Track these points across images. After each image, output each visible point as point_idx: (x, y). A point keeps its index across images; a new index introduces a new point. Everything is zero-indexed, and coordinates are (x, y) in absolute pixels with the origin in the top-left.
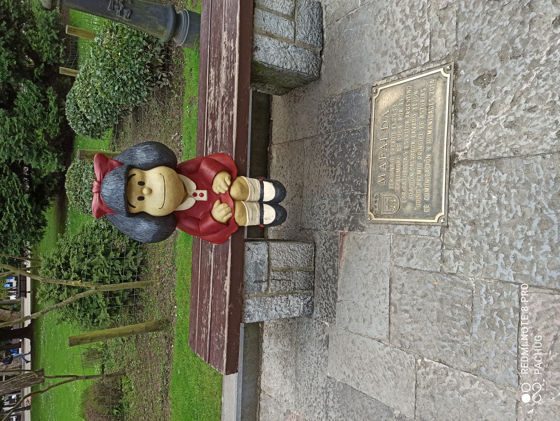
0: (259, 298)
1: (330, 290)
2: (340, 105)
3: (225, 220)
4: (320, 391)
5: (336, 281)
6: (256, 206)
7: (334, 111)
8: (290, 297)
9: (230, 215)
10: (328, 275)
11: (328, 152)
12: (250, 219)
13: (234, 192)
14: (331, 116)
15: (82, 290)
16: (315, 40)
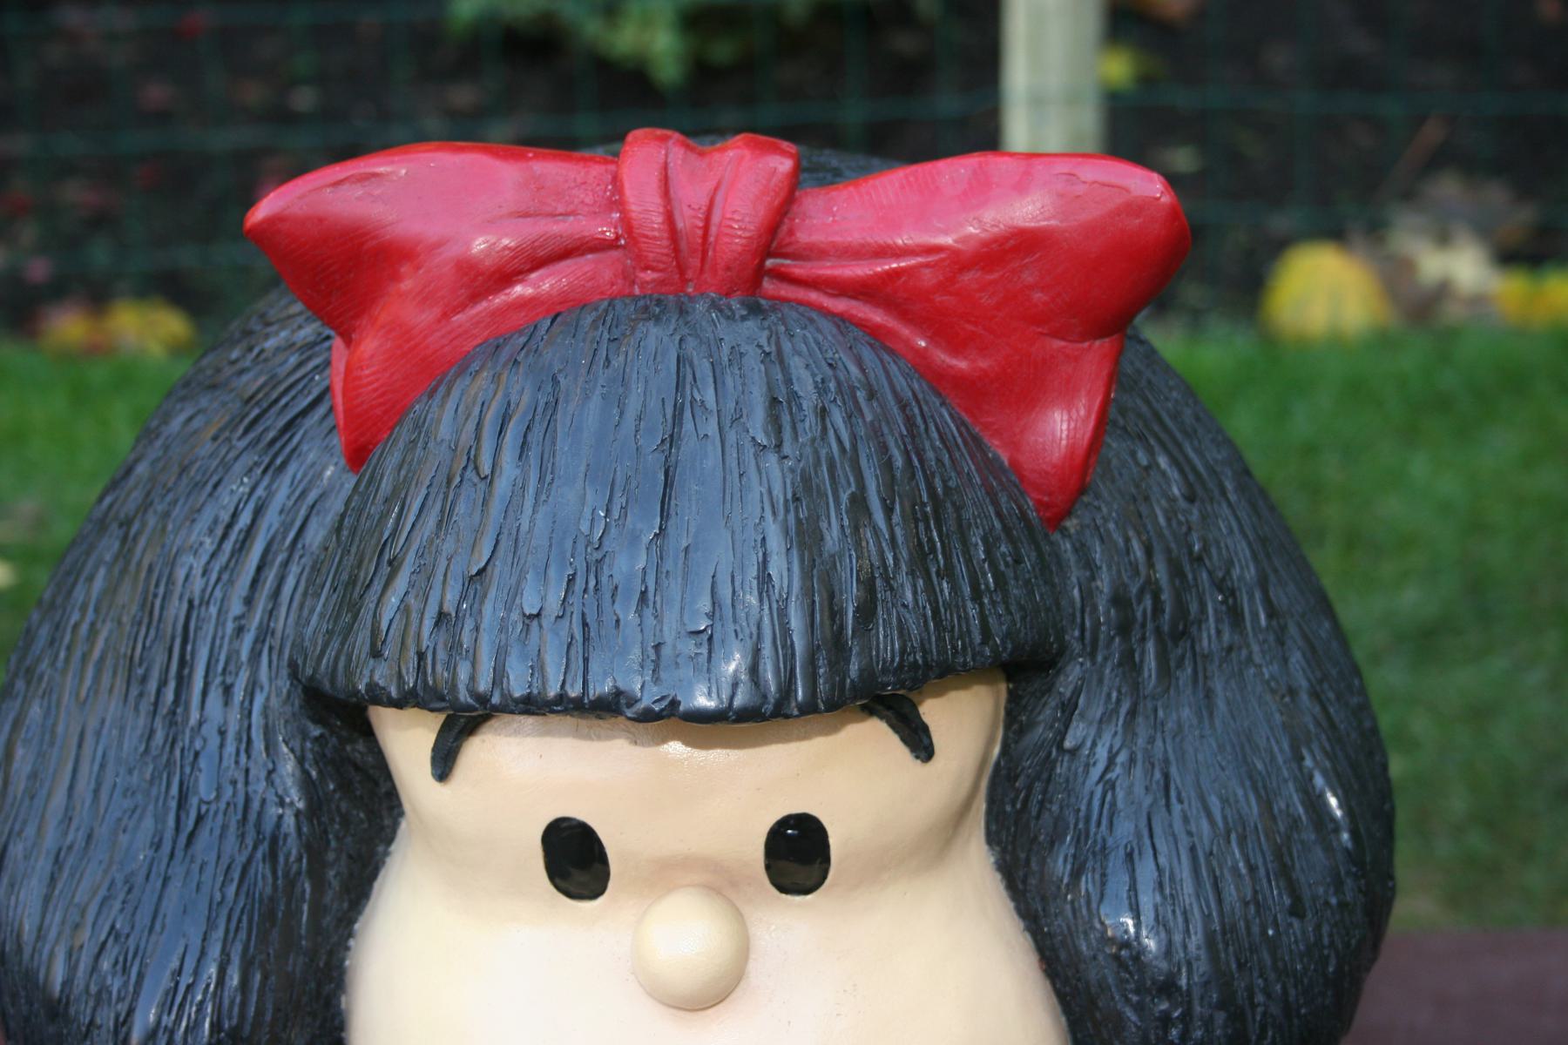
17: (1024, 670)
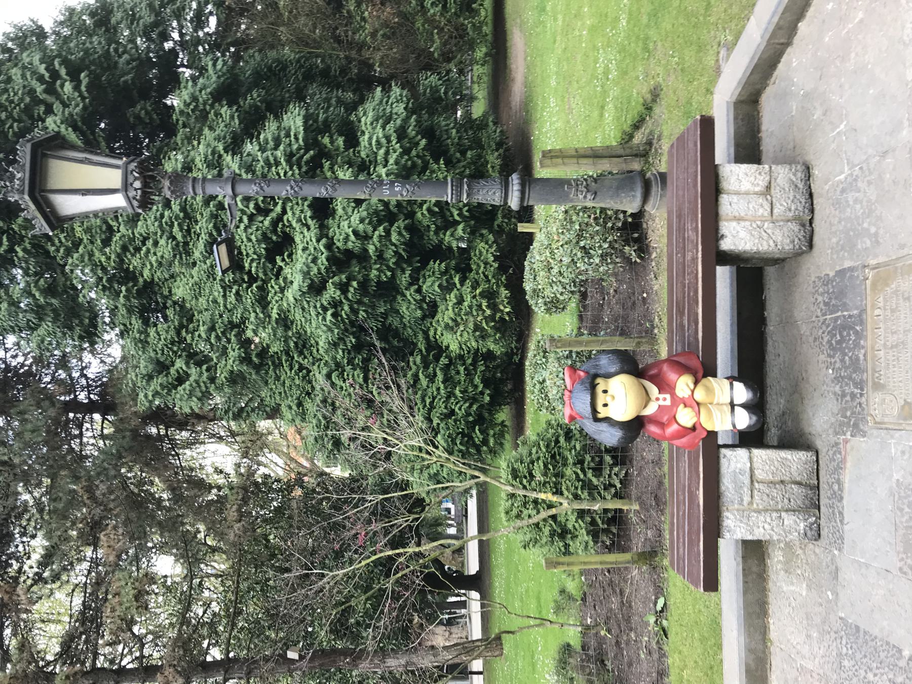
1: (836, 510)
3: (689, 425)
4: (833, 635)
5: (842, 498)
8: (783, 514)
9: (695, 420)
11: (826, 339)
15: (550, 506)
16: (801, 209)
17: (596, 376)
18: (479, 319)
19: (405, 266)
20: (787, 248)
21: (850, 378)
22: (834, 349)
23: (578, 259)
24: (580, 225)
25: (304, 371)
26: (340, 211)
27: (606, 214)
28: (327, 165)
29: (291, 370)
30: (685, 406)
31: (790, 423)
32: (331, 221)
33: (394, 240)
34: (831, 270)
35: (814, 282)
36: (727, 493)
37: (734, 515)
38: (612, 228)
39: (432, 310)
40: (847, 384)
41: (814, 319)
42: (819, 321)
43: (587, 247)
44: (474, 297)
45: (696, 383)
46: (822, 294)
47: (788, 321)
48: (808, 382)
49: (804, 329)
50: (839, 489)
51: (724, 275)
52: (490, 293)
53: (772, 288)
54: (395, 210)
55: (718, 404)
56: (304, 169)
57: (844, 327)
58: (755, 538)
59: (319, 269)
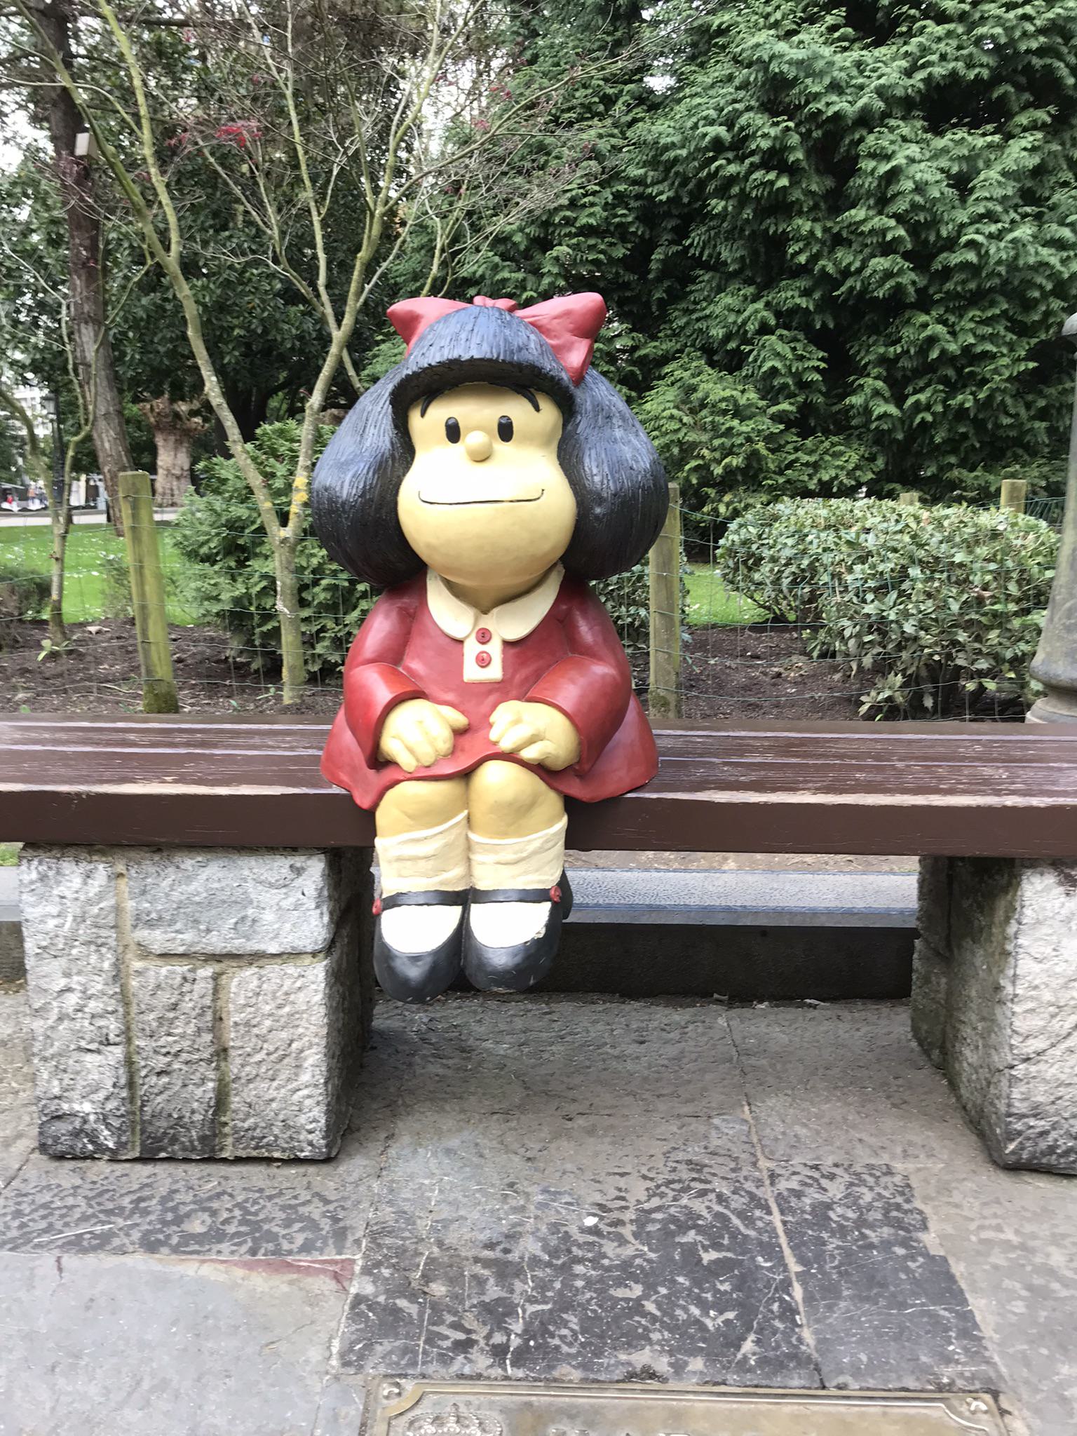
0: (111, 920)
1: (120, 1222)
2: (900, 1251)
3: (391, 744)
6: (452, 880)
7: (872, 1227)
8: (118, 1052)
9: (407, 762)
10: (188, 1215)
11: (699, 1206)
12: (405, 855)
13: (498, 780)
14: (850, 1214)
18: (705, 452)
19: (817, 295)
20: (1016, 1094)
21: (565, 1304)
22: (667, 1236)
23: (873, 566)
24: (961, 565)
25: (601, 108)
26: (940, 143)
27: (989, 628)
28: (1042, 115)
29: (606, 80)
30: (459, 733)
31: (435, 1068)
32: (919, 124)
33: (874, 261)
34: (943, 1237)
35: (889, 1172)
36: (171, 874)
37: (101, 896)
38: (955, 643)
39: (728, 359)
40: (542, 1286)
41: (764, 1164)
42: (759, 1183)
43: (906, 585)
44: (749, 439)
45: (541, 769)
46: (851, 1200)
47: (749, 1076)
48: (556, 1136)
49: (727, 1130)
50: (188, 1238)
51: (886, 887)
52: (755, 476)
53: (842, 1028)
54: (937, 265)
55: (469, 847)
56: (1037, 62)
57: (746, 1280)
58: (30, 963)
59: (816, 97)
